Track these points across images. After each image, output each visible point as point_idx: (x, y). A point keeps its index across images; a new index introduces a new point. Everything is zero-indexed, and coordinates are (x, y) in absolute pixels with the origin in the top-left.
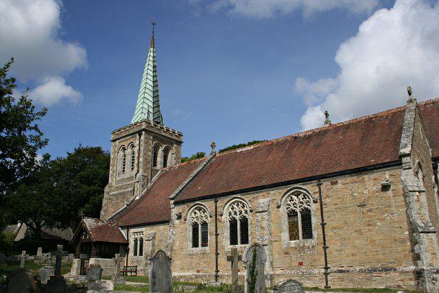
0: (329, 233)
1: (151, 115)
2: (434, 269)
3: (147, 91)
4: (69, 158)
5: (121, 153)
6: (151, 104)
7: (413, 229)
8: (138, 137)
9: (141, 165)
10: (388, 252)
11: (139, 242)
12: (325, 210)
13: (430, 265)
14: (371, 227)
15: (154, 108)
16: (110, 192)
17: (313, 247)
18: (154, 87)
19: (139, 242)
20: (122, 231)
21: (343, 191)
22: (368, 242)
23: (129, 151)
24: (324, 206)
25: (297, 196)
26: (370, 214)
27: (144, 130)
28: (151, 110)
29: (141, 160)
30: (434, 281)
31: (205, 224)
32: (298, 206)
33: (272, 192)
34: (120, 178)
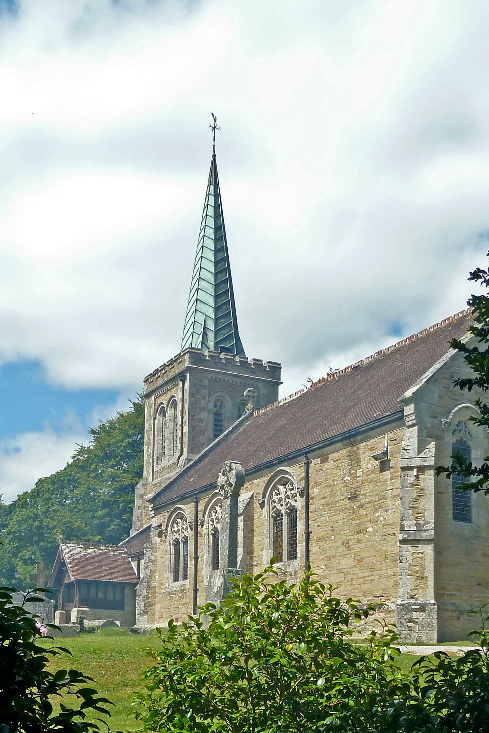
0: (314, 549)
1: (211, 336)
2: (414, 604)
3: (203, 284)
4: (100, 445)
5: (160, 418)
6: (211, 313)
7: (69, 693)
8: (180, 383)
9: (186, 439)
10: (377, 577)
11: (285, 519)
12: (311, 508)
13: (411, 597)
14: (360, 536)
15: (216, 321)
16: (145, 494)
17: (296, 572)
18: (216, 275)
19: (285, 519)
20: (132, 563)
21: (331, 471)
22: (356, 561)
23: (169, 413)
24: (311, 502)
25: (284, 485)
26: (362, 512)
27: (188, 369)
28: (211, 325)
29: (186, 429)
30: (411, 625)
31: (292, 511)
32: (284, 504)
33: (255, 481)
34: (160, 466)
